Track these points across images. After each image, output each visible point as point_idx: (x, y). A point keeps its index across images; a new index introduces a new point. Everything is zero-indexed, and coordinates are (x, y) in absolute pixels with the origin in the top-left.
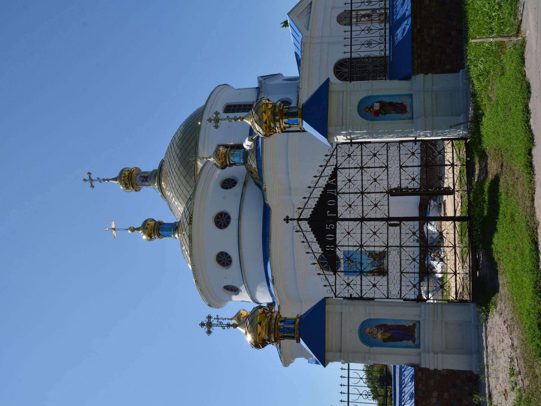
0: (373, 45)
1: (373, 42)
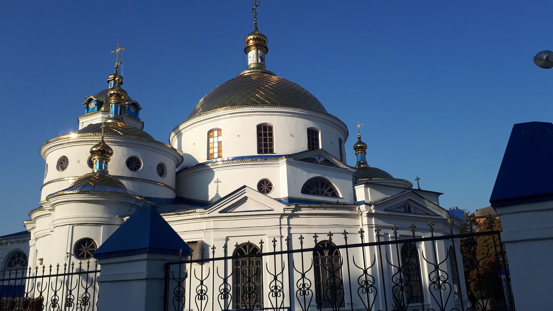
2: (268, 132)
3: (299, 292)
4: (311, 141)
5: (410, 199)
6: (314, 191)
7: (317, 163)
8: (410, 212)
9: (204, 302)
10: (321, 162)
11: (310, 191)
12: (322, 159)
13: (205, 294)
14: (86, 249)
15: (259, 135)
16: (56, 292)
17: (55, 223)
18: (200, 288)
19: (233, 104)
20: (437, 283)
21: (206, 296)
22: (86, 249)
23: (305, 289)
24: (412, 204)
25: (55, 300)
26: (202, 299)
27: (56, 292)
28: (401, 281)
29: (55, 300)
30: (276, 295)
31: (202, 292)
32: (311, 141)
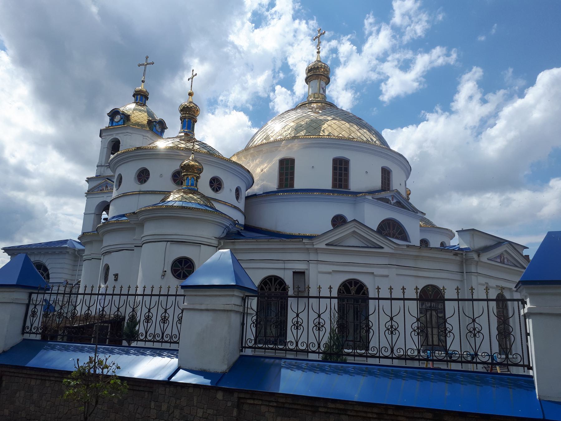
0: (389, 337)
1: (300, 332)
2: (343, 166)
3: (315, 327)
4: (387, 182)
5: (506, 251)
6: (386, 232)
7: (391, 204)
8: (504, 263)
9: (166, 325)
10: (394, 203)
11: (383, 232)
12: (395, 201)
13: (151, 319)
14: (182, 269)
15: (334, 168)
16: (89, 307)
17: (143, 239)
18: (147, 314)
19: (543, 71)
20: (473, 332)
21: (301, 327)
22: (182, 269)
23: (476, 332)
24: (506, 255)
25: (34, 311)
26: (148, 322)
27: (89, 307)
28: (418, 328)
29: (34, 311)
30: (297, 328)
31: (165, 318)
32: (387, 182)
